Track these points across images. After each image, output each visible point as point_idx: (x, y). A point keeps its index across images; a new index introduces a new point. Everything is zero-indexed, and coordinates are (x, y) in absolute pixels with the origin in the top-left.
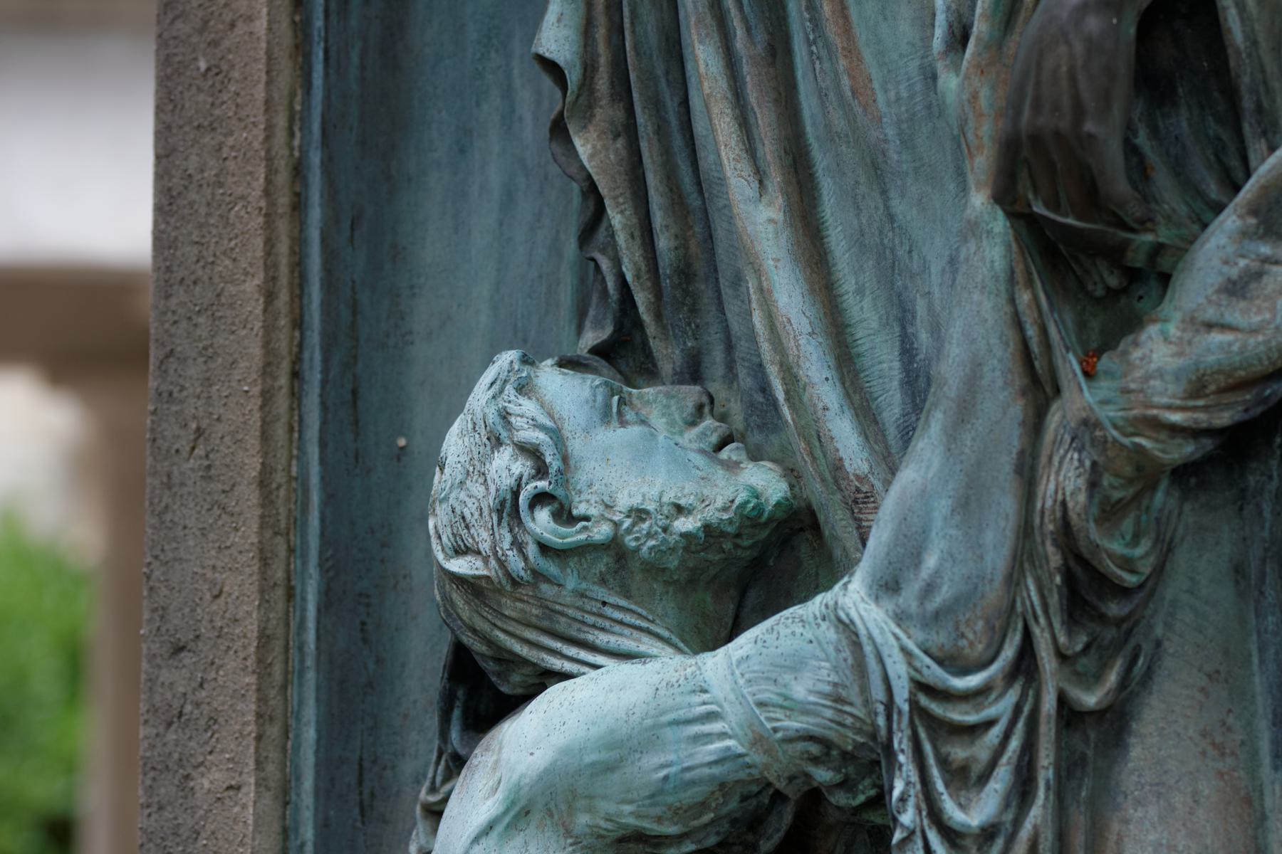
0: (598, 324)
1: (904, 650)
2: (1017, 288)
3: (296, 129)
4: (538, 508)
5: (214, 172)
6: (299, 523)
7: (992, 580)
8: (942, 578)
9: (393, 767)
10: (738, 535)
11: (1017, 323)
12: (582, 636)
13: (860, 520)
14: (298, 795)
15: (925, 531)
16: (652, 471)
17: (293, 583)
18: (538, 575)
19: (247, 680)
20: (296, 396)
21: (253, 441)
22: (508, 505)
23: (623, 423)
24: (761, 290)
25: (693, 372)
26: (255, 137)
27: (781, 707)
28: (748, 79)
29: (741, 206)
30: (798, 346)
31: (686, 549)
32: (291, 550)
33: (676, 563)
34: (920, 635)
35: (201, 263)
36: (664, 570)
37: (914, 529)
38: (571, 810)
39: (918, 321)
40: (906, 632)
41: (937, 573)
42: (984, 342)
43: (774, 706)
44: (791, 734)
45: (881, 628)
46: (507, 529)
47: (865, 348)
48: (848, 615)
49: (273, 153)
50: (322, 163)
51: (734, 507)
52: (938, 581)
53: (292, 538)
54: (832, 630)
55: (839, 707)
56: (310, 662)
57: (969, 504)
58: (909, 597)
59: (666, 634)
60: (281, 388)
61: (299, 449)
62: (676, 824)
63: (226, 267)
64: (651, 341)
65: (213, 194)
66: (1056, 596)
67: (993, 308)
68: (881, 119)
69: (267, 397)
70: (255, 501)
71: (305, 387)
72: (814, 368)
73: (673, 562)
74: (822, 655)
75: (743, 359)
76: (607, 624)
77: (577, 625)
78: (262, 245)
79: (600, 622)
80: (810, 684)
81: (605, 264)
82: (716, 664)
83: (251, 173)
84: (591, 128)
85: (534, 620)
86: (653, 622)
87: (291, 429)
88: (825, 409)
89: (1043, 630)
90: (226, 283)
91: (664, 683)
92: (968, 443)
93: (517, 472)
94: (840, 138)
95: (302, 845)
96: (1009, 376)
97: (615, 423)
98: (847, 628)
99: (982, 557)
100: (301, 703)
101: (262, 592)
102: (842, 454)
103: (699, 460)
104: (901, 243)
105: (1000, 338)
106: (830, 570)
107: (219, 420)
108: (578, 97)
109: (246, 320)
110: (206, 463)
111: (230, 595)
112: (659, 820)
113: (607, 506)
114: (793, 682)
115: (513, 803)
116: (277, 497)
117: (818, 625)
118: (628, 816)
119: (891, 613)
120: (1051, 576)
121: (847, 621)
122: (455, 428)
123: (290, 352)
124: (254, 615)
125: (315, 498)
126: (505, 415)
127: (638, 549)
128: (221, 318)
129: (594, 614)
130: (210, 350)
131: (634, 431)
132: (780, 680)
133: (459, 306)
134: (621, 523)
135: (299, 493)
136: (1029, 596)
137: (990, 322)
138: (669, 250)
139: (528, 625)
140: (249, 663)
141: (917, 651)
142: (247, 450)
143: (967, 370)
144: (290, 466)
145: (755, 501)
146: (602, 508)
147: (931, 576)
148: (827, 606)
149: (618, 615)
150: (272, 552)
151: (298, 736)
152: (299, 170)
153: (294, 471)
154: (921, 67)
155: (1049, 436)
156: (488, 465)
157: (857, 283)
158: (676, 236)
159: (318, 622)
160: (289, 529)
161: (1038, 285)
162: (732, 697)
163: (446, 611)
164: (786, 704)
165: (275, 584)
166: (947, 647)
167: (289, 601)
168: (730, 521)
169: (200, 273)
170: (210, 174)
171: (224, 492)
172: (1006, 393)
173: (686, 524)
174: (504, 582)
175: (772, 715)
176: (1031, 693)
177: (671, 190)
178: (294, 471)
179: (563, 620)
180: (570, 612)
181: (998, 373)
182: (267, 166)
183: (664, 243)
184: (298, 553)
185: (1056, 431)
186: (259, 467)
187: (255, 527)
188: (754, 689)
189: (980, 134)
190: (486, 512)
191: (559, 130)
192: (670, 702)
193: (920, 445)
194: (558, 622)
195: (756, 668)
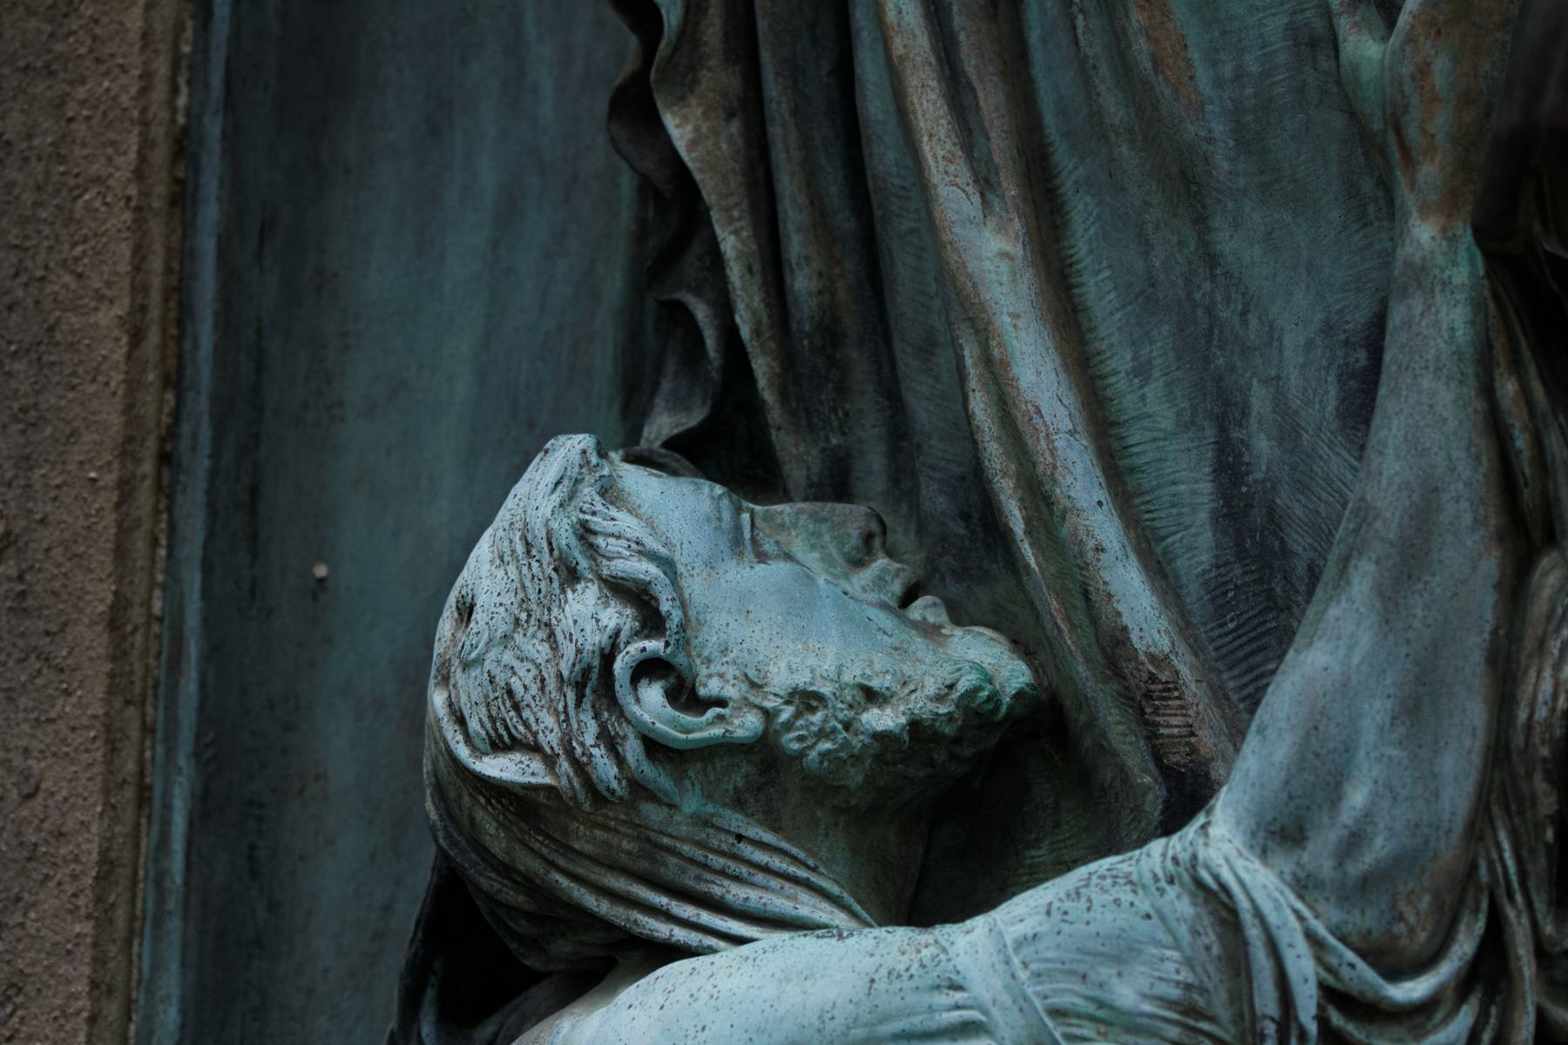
0: (678, 403)
1: (1310, 936)
2: (1497, 372)
3: (182, 81)
4: (644, 682)
5: (49, 140)
6: (162, 688)
7: (1450, 831)
8: (1375, 824)
10: (957, 740)
11: (1495, 426)
12: (702, 887)
13: (1157, 725)
15: (1348, 749)
16: (808, 632)
17: (148, 780)
18: (639, 789)
19: (77, 929)
20: (166, 492)
21: (102, 559)
22: (594, 675)
23: (762, 557)
24: (987, 360)
25: (836, 485)
26: (125, 89)
27: (1092, 1019)
28: (962, 37)
29: (957, 230)
30: (1053, 451)
31: (879, 758)
32: (148, 730)
33: (860, 778)
34: (1335, 915)
35: (23, 278)
36: (838, 789)
37: (1331, 745)
39: (1253, 422)
40: (1311, 908)
41: (1368, 816)
42: (1442, 454)
43: (1079, 1016)
45: (1275, 900)
46: (590, 714)
47: (1145, 459)
48: (1216, 878)
49: (150, 115)
50: (224, 134)
51: (955, 695)
52: (1369, 829)
53: (149, 710)
54: (1186, 900)
55: (1192, 1023)
56: (173, 903)
57: (1417, 709)
58: (1319, 854)
59: (835, 890)
60: (144, 477)
61: (166, 572)
63: (65, 286)
64: (773, 432)
65: (47, 173)
66: (1543, 861)
67: (1455, 401)
68: (1202, 105)
69: (126, 489)
70: (102, 651)
71: (182, 478)
72: (1079, 485)
73: (855, 777)
74: (1168, 939)
75: (933, 468)
76: (744, 870)
77: (694, 871)
78: (128, 254)
79: (733, 866)
80: (1144, 985)
81: (702, 312)
82: (972, 944)
83: (113, 143)
84: (693, 101)
85: (624, 859)
86: (814, 869)
87: (155, 542)
88: (1099, 549)
89: (1519, 915)
90: (66, 310)
91: (883, 972)
92: (1419, 612)
93: (612, 625)
94: (1117, 134)
96: (1482, 511)
97: (750, 555)
98: (1218, 902)
99: (1437, 795)
100: (156, 966)
101: (106, 792)
102: (1126, 620)
103: (883, 619)
104: (1228, 300)
105: (1468, 450)
106: (1187, 797)
107: (43, 521)
108: (673, 53)
109: (97, 370)
110: (19, 588)
111: (52, 794)
113: (753, 685)
114: (1115, 981)
116: (132, 645)
117: (1162, 891)
119: (1288, 877)
120: (1539, 828)
121: (1215, 886)
122: (484, 548)
123: (158, 424)
124: (94, 829)
125: (193, 650)
126: (585, 532)
127: (802, 754)
128: (53, 364)
129: (723, 854)
130: (33, 413)
131: (780, 569)
132: (1092, 975)
134: (777, 712)
135: (165, 641)
136: (1502, 859)
137: (1452, 424)
138: (810, 294)
139: (614, 867)
140: (81, 902)
141: (1332, 940)
142: (91, 571)
143: (1415, 497)
144: (150, 598)
145: (989, 687)
146: (745, 687)
147: (1357, 820)
148: (1175, 860)
149: (761, 857)
150: (122, 730)
151: (148, 1018)
152: (184, 145)
153: (157, 606)
154: (1290, 27)
155: (1538, 608)
156: (555, 611)
157: (1134, 359)
158: (820, 274)
159: (189, 843)
160: (144, 696)
161: (1532, 369)
162: (1005, 999)
163: (449, 836)
164: (1101, 1013)
165: (125, 781)
166: (1375, 935)
167: (140, 807)
168: (950, 717)
169: (20, 293)
170: (43, 141)
171: (47, 633)
172: (1477, 537)
174: (581, 796)
175: (1076, 1031)
176: (1494, 1010)
177: (812, 203)
178: (157, 606)
179: (672, 860)
180: (686, 848)
181: (1464, 505)
182: (141, 134)
183: (802, 283)
184: (160, 734)
185: (1553, 600)
186: (110, 598)
187: (100, 690)
188: (1045, 988)
189: (1431, 129)
190: (552, 684)
191: (634, 107)
192: (897, 1002)
193: (1333, 612)
194: (666, 866)
195: (1050, 954)
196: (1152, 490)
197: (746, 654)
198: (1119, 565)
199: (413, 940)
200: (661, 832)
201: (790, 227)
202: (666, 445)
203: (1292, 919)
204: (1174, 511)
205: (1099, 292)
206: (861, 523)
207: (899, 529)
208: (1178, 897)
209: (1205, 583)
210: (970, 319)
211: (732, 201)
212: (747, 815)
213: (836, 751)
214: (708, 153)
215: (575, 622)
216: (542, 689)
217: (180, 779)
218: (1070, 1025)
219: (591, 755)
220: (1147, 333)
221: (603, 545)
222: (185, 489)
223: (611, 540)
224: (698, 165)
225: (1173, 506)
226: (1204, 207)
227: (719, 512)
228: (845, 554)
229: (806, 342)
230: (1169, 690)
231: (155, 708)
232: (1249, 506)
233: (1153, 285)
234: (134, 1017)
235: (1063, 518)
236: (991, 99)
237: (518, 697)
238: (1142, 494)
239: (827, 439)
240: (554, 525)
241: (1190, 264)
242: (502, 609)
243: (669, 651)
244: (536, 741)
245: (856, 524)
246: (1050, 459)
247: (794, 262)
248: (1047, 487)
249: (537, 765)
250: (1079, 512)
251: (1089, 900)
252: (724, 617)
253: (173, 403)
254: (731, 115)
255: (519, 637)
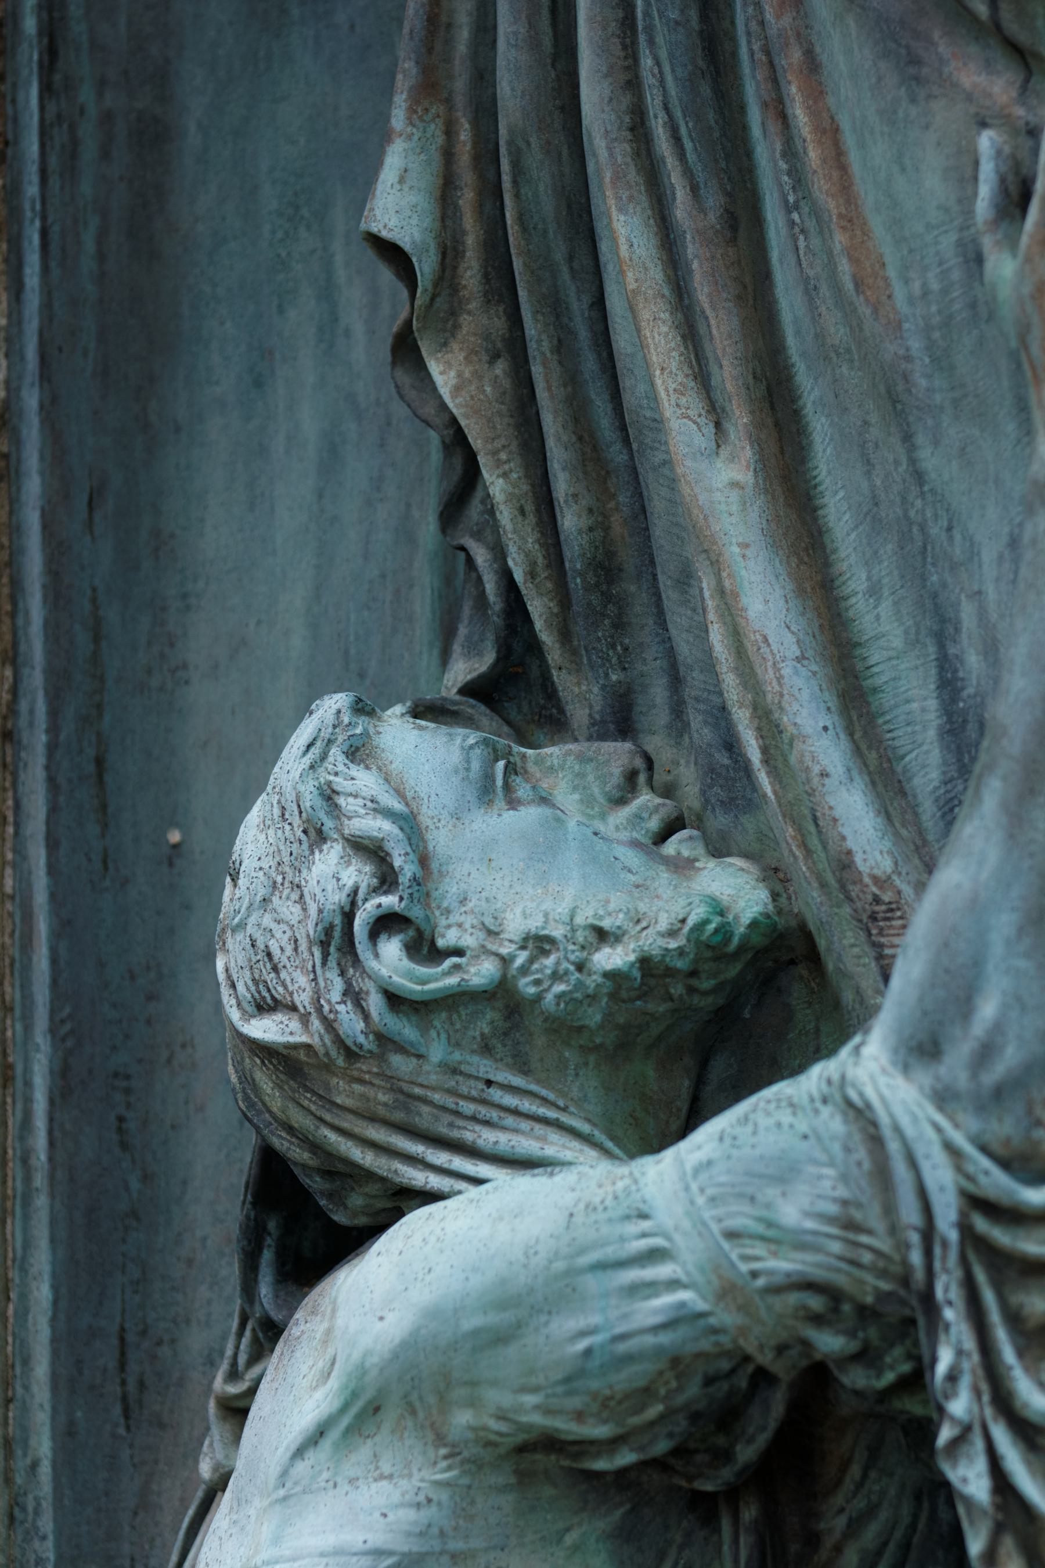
0: (472, 649)
4: (383, 937)
6: (17, 965)
9: (173, 1341)
10: (693, 973)
12: (455, 1134)
14: (26, 1388)
15: (977, 963)
17: (10, 1059)
18: (385, 1041)
22: (337, 933)
23: (513, 803)
27: (763, 1238)
28: (695, 265)
29: (688, 463)
30: (779, 679)
31: (613, 996)
33: (598, 1018)
34: (973, 1124)
36: (580, 1029)
38: (444, 1404)
39: (964, 636)
40: (952, 1119)
41: (998, 1028)
44: (778, 1280)
47: (884, 678)
48: (861, 1095)
50: (42, 407)
51: (686, 929)
56: (40, 1180)
59: (585, 1128)
61: (15, 851)
62: (605, 1422)
64: (555, 673)
68: (899, 326)
71: (23, 754)
72: (804, 712)
73: (594, 1017)
75: (697, 699)
76: (494, 1115)
77: (447, 1118)
79: (483, 1111)
81: (481, 556)
84: (455, 346)
85: (381, 1111)
86: (564, 1109)
88: (824, 774)
91: (582, 1206)
95: (35, 1465)
97: (500, 802)
98: (860, 1115)
100: (27, 1245)
102: (850, 844)
103: (631, 857)
104: (936, 516)
112: (580, 1416)
113: (490, 933)
115: (355, 1395)
117: (816, 1111)
118: (531, 1411)
122: (254, 816)
125: (42, 927)
126: (329, 795)
127: (539, 998)
131: (530, 814)
132: (759, 1197)
133: (259, 623)
134: (512, 958)
135: (18, 920)
138: (580, 532)
139: (373, 1119)
146: (482, 935)
148: (829, 1082)
151: (24, 1296)
157: (869, 579)
158: (590, 511)
162: (686, 1224)
163: (247, 1098)
164: (771, 1233)
168: (681, 952)
173: (612, 958)
174: (334, 1053)
175: (749, 1251)
177: (580, 439)
179: (425, 1109)
180: (437, 1097)
183: (571, 521)
184: (18, 1012)
190: (303, 946)
191: (405, 349)
195: (723, 1179)
196: (891, 709)
197: (483, 903)
198: (843, 788)
199: (244, 1203)
200: (412, 1083)
201: (556, 466)
202: (462, 691)
203: (931, 1134)
204: (909, 729)
205: (838, 513)
206: (625, 760)
207: (682, 762)
208: (832, 1116)
209: (937, 800)
210: (705, 551)
211: (498, 444)
212: (496, 1060)
213: (570, 992)
214: (472, 397)
215: (318, 882)
216: (296, 949)
217: (38, 1056)
218: (743, 1246)
219: (337, 1012)
220: (876, 552)
221: (343, 804)
222: (26, 765)
223: (351, 800)
224: (463, 410)
225: (908, 724)
226: (908, 424)
227: (468, 762)
228: (606, 793)
229: (578, 580)
230: (892, 910)
231: (13, 986)
232: (965, 721)
233: (876, 504)
234: (12, 1295)
235: (791, 745)
236: (722, 328)
237: (276, 959)
238: (883, 714)
239: (607, 675)
240: (301, 788)
241: (904, 481)
242: (261, 873)
243: (403, 904)
244: (292, 1001)
245: (620, 762)
246: (777, 688)
247: (562, 500)
248: (776, 715)
249: (295, 1025)
250: (804, 738)
251: (756, 1125)
252: (467, 867)
253: (11, 680)
254: (494, 357)
255: (275, 900)
